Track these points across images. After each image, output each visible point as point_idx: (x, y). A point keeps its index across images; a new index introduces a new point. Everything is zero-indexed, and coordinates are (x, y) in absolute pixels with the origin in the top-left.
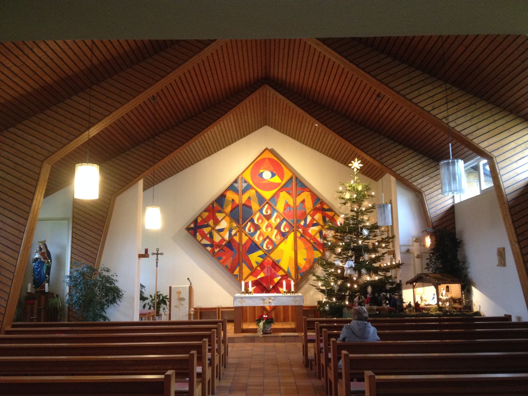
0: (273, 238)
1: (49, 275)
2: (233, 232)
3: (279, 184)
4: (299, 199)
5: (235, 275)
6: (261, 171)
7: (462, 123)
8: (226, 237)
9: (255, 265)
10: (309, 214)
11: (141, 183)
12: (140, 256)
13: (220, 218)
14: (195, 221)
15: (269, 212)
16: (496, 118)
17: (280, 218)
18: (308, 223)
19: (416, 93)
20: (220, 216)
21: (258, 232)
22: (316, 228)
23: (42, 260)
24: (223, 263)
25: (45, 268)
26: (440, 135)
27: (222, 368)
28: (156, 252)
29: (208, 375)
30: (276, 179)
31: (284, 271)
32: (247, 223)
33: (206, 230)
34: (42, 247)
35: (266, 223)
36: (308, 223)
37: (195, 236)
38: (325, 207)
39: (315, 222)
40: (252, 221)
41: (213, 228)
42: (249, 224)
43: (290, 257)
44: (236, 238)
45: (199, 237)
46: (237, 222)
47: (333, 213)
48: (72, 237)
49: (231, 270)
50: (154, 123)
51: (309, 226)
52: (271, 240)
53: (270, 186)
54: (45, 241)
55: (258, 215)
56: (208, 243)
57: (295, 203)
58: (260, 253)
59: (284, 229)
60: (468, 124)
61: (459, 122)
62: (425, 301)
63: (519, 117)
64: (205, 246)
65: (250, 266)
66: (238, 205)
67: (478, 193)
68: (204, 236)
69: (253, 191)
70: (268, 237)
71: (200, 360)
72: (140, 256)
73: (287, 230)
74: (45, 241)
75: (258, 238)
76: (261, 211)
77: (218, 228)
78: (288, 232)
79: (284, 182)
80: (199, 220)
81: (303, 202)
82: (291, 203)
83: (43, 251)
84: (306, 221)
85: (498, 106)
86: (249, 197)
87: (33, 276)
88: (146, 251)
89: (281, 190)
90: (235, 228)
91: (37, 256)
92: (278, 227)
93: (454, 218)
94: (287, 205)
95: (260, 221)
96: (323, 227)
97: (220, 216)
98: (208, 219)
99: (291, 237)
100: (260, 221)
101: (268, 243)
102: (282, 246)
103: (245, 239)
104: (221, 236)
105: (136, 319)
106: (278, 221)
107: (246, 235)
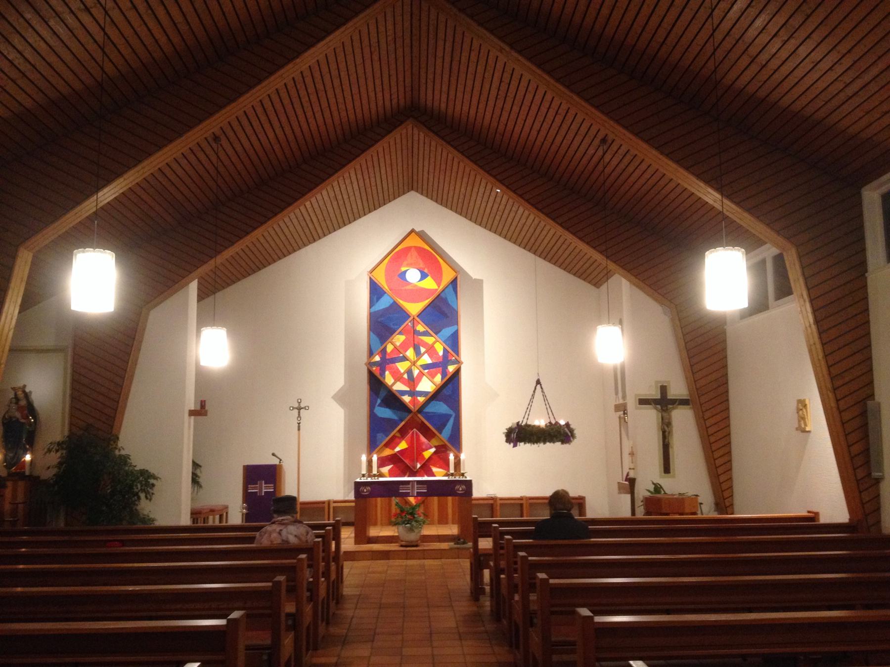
6: (403, 269)
71: (292, 590)
79: (441, 287)
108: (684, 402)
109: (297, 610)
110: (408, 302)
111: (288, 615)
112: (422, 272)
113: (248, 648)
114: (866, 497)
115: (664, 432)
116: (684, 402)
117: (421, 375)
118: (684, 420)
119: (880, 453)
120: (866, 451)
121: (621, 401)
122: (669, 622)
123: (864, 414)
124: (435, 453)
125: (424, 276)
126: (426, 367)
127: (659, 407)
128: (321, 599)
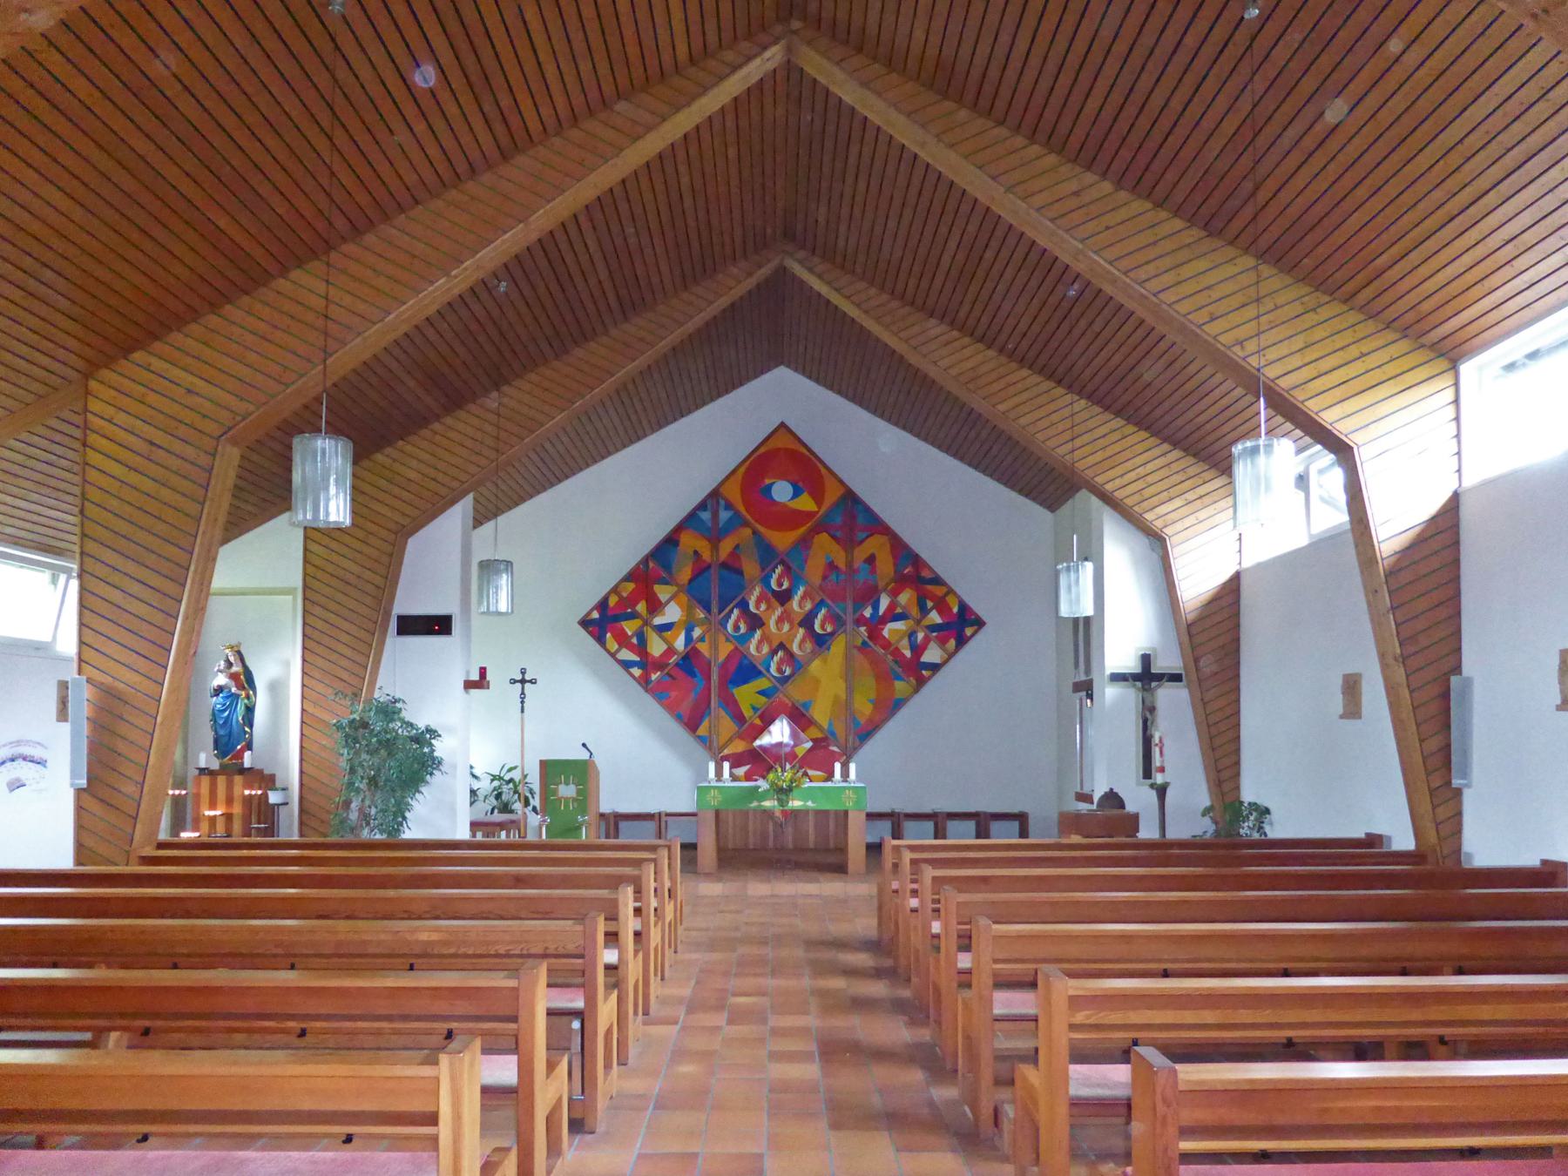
0: (795, 648)
1: (251, 726)
2: (697, 633)
3: (810, 515)
4: (861, 553)
5: (699, 737)
6: (768, 481)
7: (1278, 363)
8: (680, 643)
9: (747, 713)
10: (885, 590)
11: (466, 504)
12: (469, 685)
13: (663, 597)
14: (602, 605)
15: (786, 585)
16: (1365, 347)
17: (812, 599)
18: (881, 612)
19: (1168, 279)
20: (663, 592)
21: (758, 634)
22: (900, 626)
23: (234, 690)
24: (671, 707)
25: (240, 709)
26: (1223, 389)
27: (669, 953)
28: (519, 677)
29: (633, 971)
30: (806, 503)
31: (820, 728)
32: (731, 611)
33: (630, 627)
34: (232, 659)
35: (779, 611)
36: (881, 612)
37: (601, 640)
38: (925, 574)
39: (899, 610)
40: (743, 605)
41: (646, 623)
42: (736, 612)
43: (836, 697)
44: (703, 648)
45: (613, 646)
46: (707, 609)
47: (944, 589)
48: (304, 635)
49: (692, 725)
50: (499, 350)
51: (884, 620)
52: (790, 655)
53: (790, 519)
54: (239, 644)
55: (757, 592)
56: (635, 658)
57: (849, 564)
58: (762, 683)
59: (823, 627)
60: (1296, 361)
61: (1272, 354)
62: (293, 524)
63: (1423, 346)
64: (626, 665)
65: (739, 718)
66: (709, 567)
67: (1302, 541)
68: (622, 640)
69: (747, 532)
70: (782, 646)
71: (612, 938)
72: (469, 685)
73: (829, 629)
74: (239, 644)
75: (758, 648)
76: (765, 581)
77: (658, 621)
78: (832, 634)
79: (823, 509)
80: (613, 601)
81: (871, 560)
82: (841, 562)
83: (235, 669)
84: (876, 607)
85: (1372, 317)
86: (737, 546)
87: (215, 728)
88: (483, 671)
89: (817, 530)
90: (700, 623)
91: (221, 680)
92: (807, 622)
93: (1456, 544)
94: (831, 566)
95: (763, 607)
96: (918, 622)
97: (663, 592)
98: (633, 600)
99: (838, 647)
100: (763, 607)
101: (781, 662)
102: (816, 666)
103: (725, 649)
104: (664, 640)
105: (463, 833)
106: (808, 606)
107: (727, 640)
108: (1176, 678)
109: (620, 959)
110: (769, 527)
111: (608, 967)
112: (794, 484)
113: (551, 1013)
114: (1442, 813)
115: (1145, 722)
116: (1176, 678)
117: (927, 640)
118: (1174, 702)
119: (1466, 753)
120: (1446, 749)
121: (1083, 678)
122: (1136, 989)
123: (1446, 696)
124: (810, 750)
125: (796, 494)
126: (933, 628)
127: (1139, 684)
128: (653, 945)
